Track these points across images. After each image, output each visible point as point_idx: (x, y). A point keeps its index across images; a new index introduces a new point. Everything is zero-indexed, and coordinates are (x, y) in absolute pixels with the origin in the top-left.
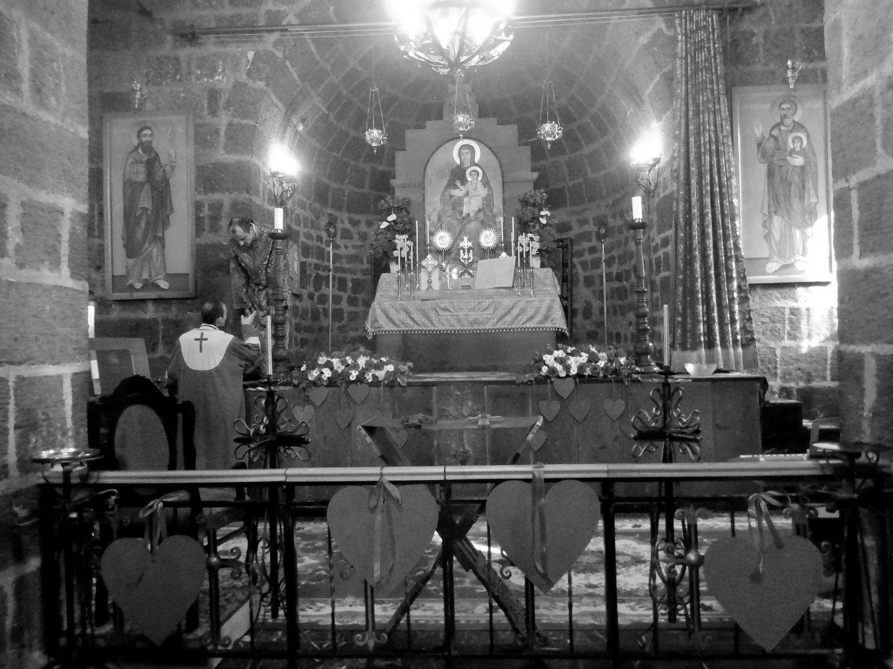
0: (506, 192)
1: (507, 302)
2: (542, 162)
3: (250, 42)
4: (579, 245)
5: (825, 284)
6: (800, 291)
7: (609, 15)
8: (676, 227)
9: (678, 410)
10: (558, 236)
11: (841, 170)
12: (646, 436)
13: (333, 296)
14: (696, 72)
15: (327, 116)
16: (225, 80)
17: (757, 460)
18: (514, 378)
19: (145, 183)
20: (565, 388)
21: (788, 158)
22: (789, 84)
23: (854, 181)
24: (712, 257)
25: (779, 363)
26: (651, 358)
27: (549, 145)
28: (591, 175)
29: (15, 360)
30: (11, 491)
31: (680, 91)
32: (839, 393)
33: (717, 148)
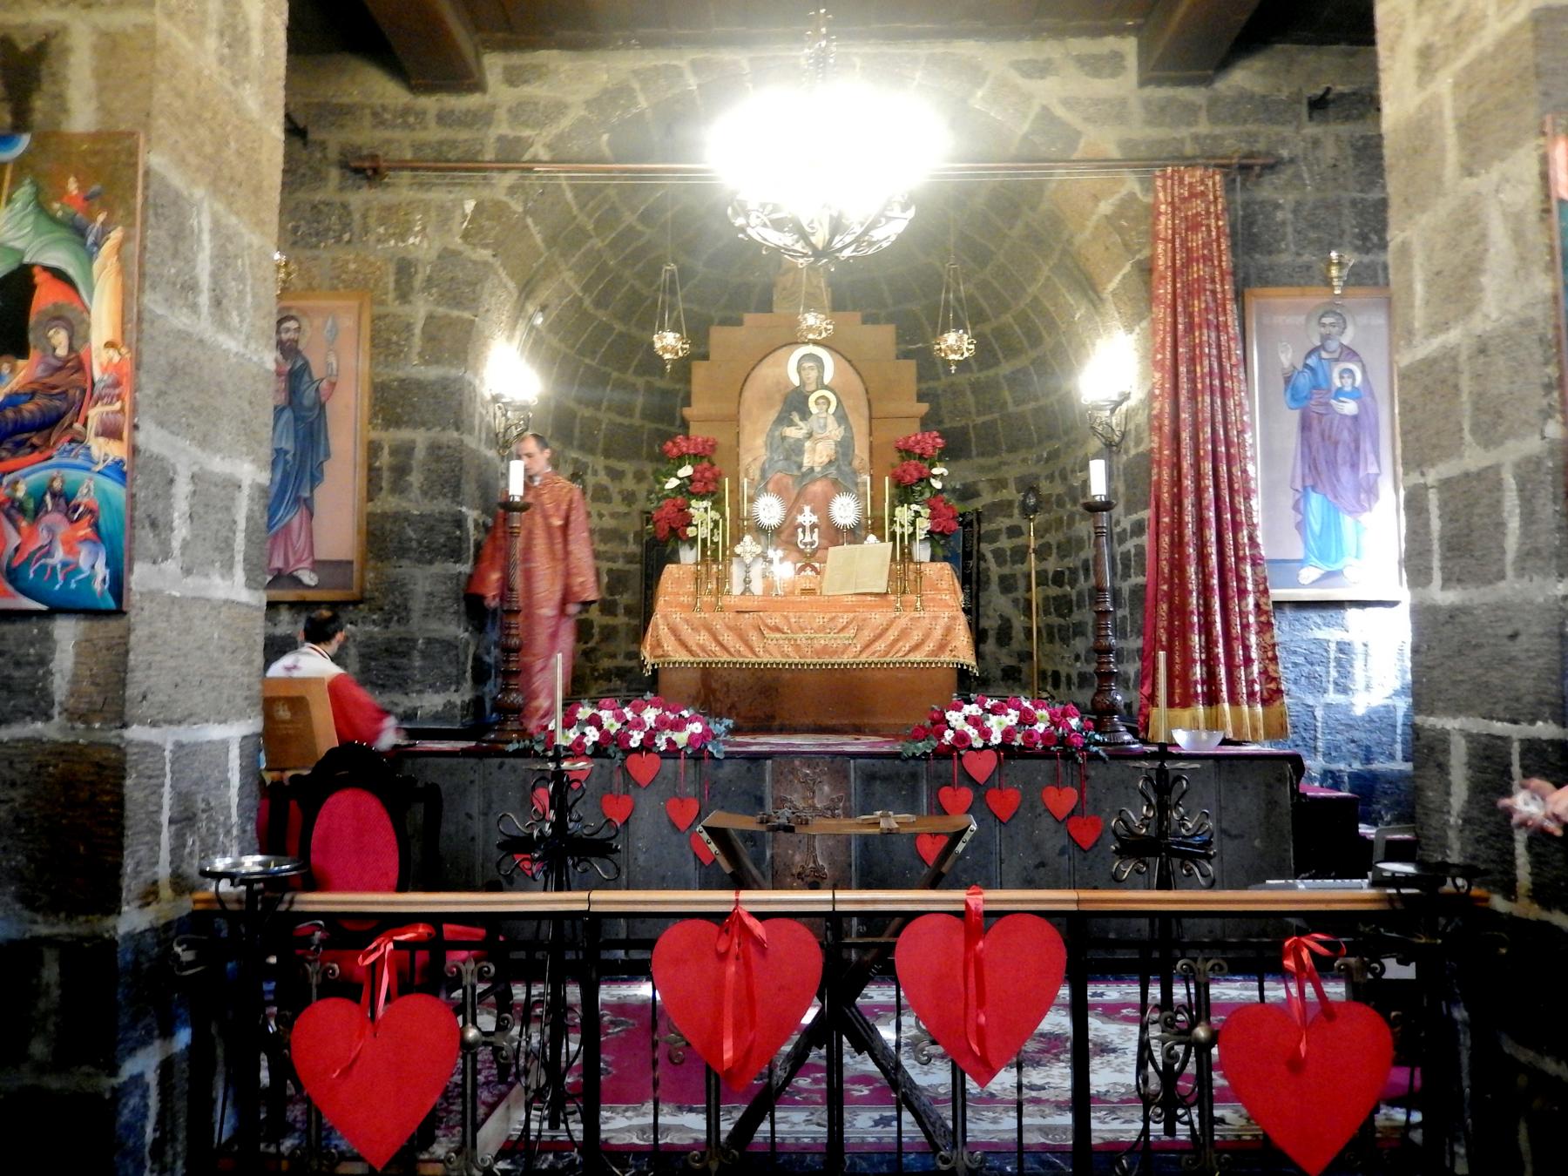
1: (878, 618)
4: (990, 521)
5: (1393, 604)
6: (1352, 614)
8: (1158, 507)
10: (960, 508)
11: (1414, 457)
12: (1132, 847)
14: (1188, 263)
15: (581, 300)
16: (425, 245)
17: (1294, 887)
18: (898, 748)
19: (283, 409)
20: (982, 767)
21: (1333, 402)
22: (1332, 287)
23: (1432, 477)
24: (1214, 558)
27: (953, 368)
28: (1011, 408)
30: (162, 922)
31: (1164, 291)
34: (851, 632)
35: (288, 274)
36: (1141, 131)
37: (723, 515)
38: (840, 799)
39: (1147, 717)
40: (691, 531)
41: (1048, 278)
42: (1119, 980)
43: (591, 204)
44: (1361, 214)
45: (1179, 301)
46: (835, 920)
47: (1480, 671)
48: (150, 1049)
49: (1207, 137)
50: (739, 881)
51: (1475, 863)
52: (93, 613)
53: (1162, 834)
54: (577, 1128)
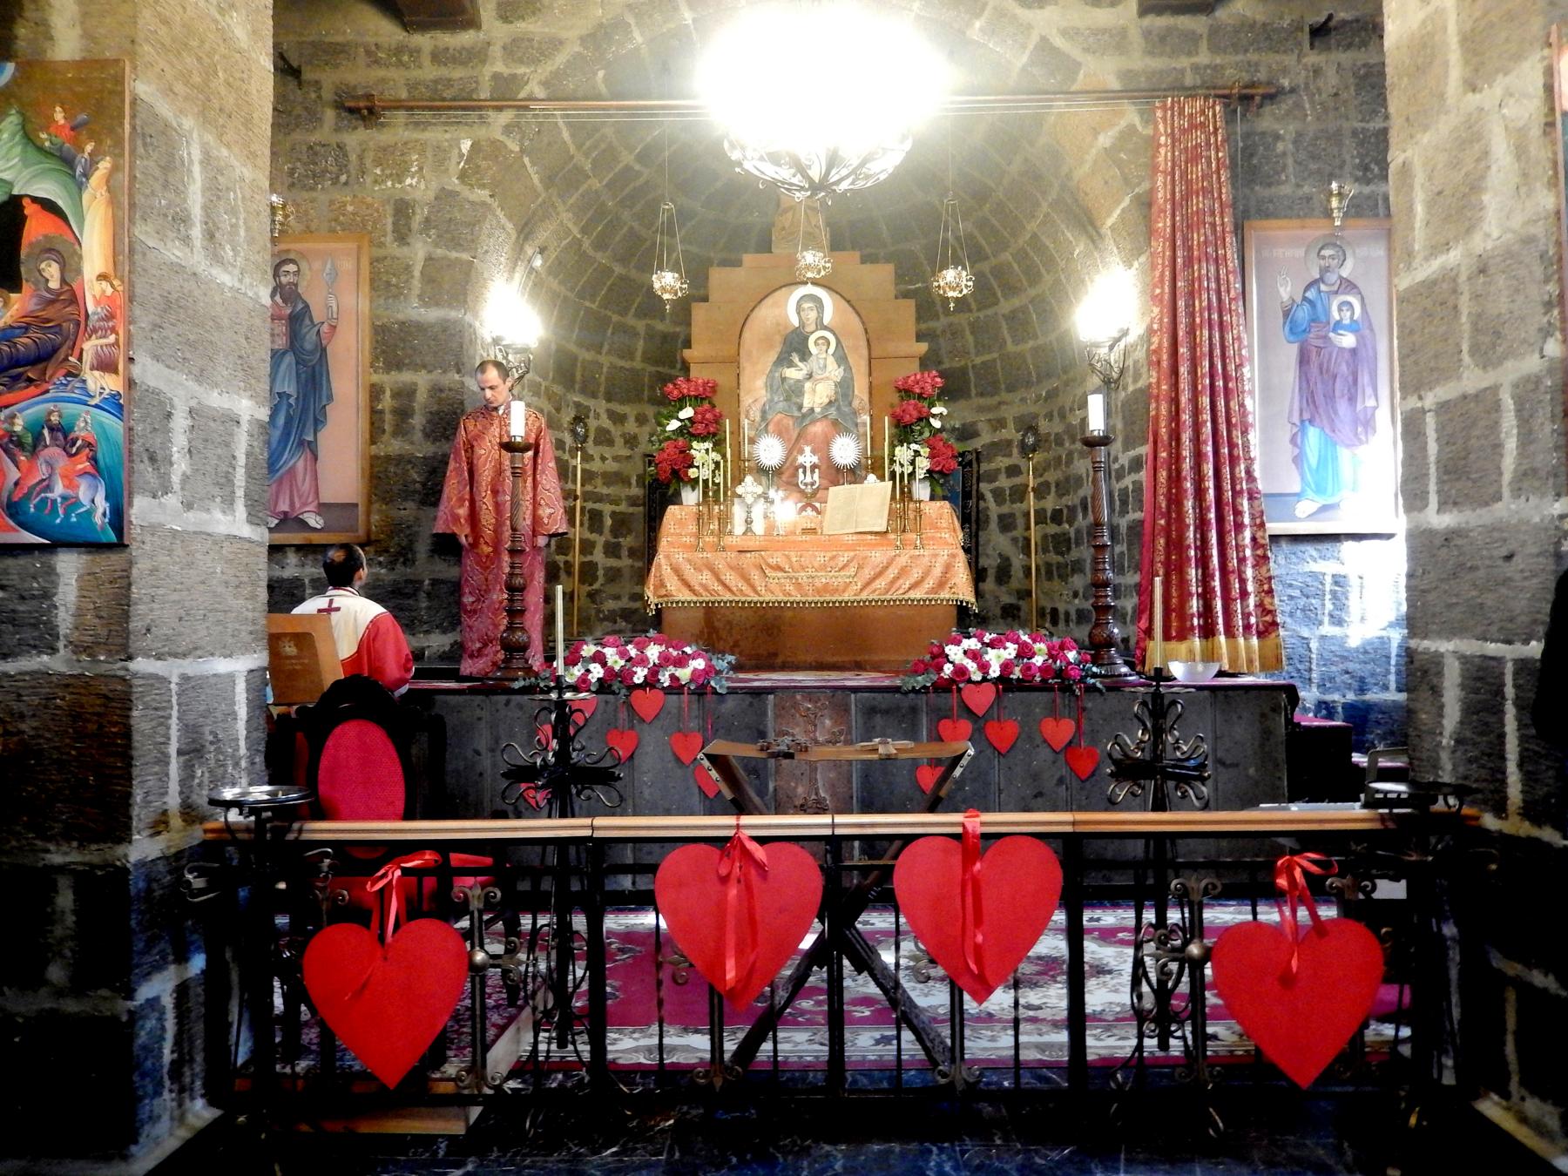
0: (874, 374)
1: (878, 556)
2: (932, 324)
3: (466, 124)
4: (990, 461)
5: (1390, 536)
6: (1348, 546)
7: (1052, 100)
8: (1155, 443)
9: (1176, 733)
10: (960, 447)
11: (1412, 383)
12: (1127, 770)
13: (581, 540)
14: (1187, 197)
15: (579, 243)
16: (422, 186)
17: (1289, 809)
18: (898, 682)
19: (284, 353)
20: (981, 700)
21: (1332, 335)
23: (1430, 400)
24: (1211, 492)
25: (1314, 662)
26: (1117, 652)
27: (952, 305)
28: (1011, 347)
29: (180, 650)
30: (173, 850)
31: (1163, 224)
32: (1409, 712)
33: (1221, 316)
34: (852, 571)
35: (286, 216)
36: (1139, 61)
37: (724, 456)
38: (841, 733)
39: (1144, 650)
40: (692, 473)
41: (1047, 215)
42: (1115, 905)
43: (588, 144)
44: (1361, 144)
45: (1178, 235)
46: (835, 843)
47: (1474, 593)
48: (165, 973)
49: (1207, 67)
50: (740, 806)
51: (1467, 783)
52: (94, 547)
53: (1157, 756)
54: (585, 1049)
